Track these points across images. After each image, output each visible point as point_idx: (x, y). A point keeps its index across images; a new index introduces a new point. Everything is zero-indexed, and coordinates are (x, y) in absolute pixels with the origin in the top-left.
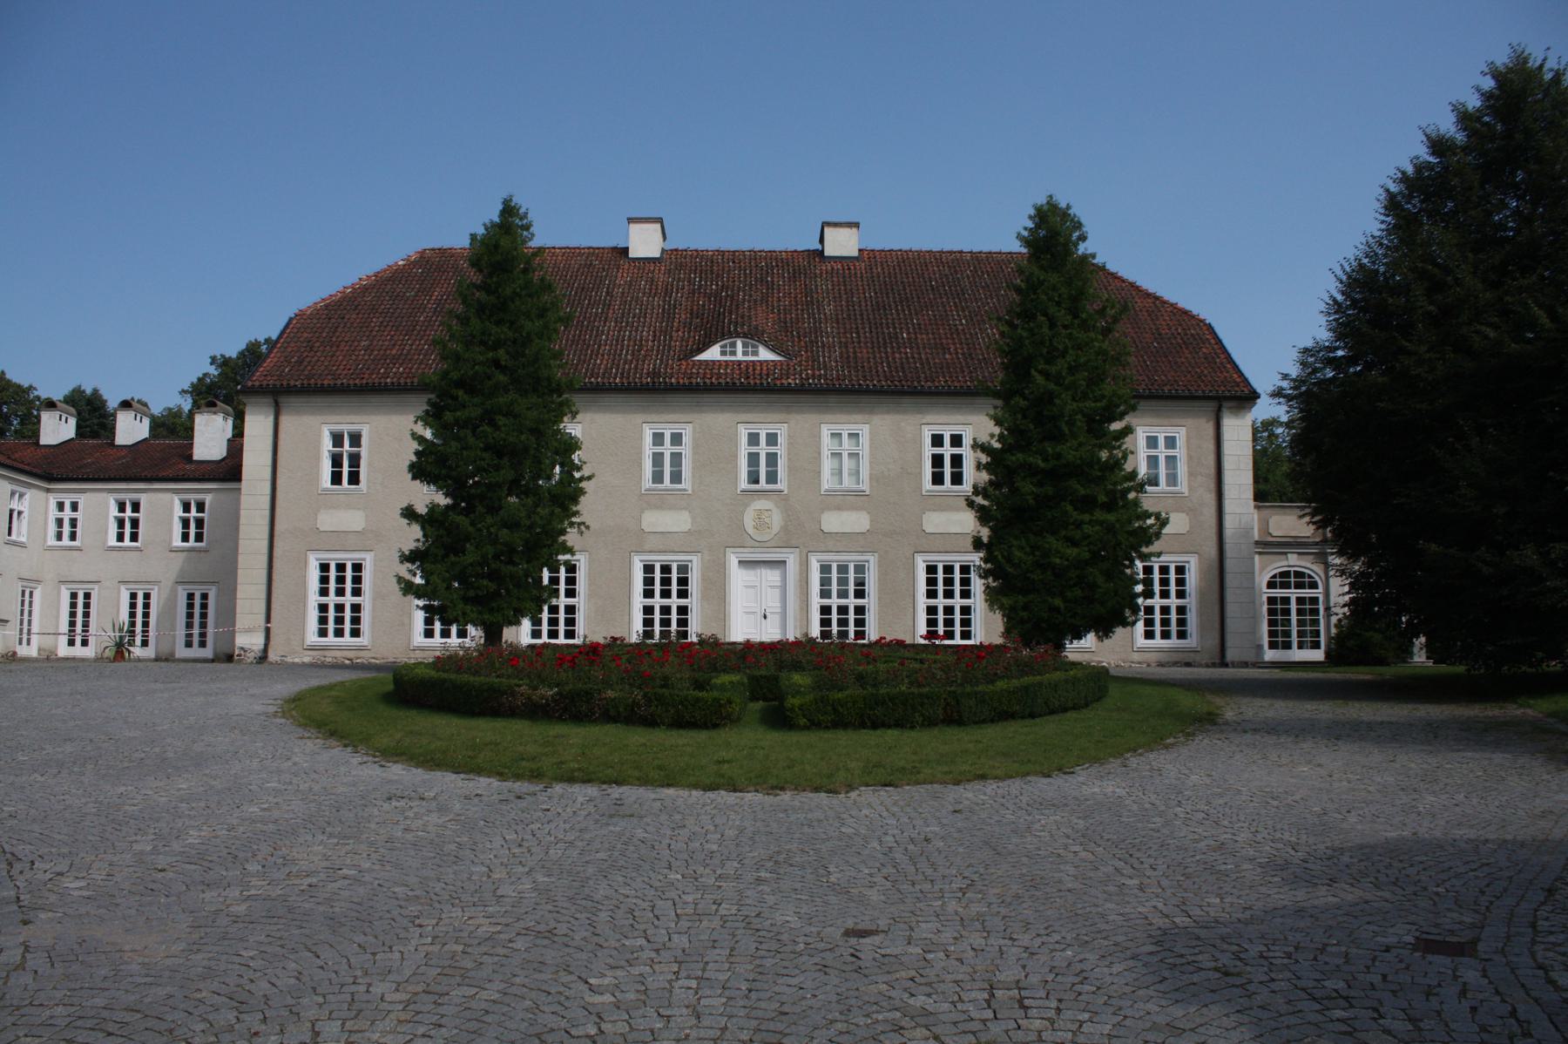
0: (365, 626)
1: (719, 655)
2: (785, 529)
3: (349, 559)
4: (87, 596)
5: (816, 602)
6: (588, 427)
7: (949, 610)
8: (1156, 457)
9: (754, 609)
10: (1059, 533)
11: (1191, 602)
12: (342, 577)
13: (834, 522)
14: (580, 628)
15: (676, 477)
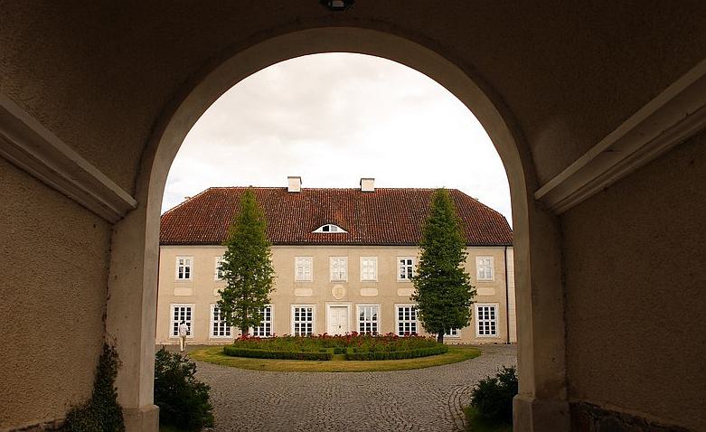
1: (325, 339)
2: (347, 295)
5: (359, 322)
9: (336, 323)
10: (443, 297)
11: (497, 320)
13: (364, 292)
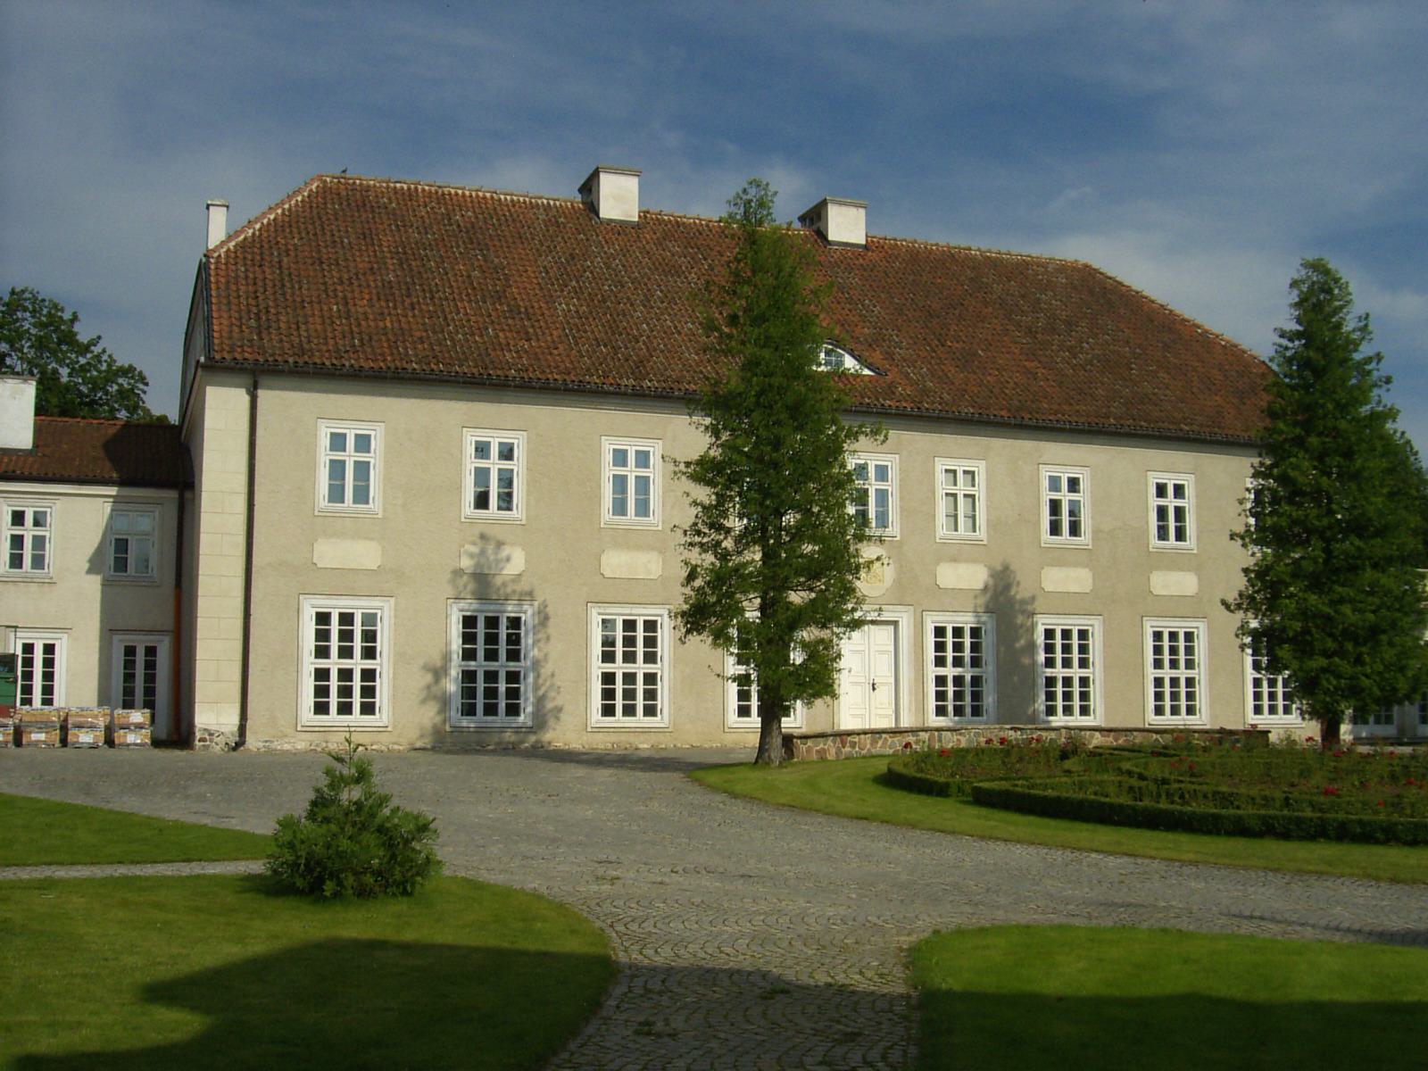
0: (663, 700)
3: (1181, 627)
4: (49, 649)
5: (932, 671)
6: (862, 454)
7: (346, 674)
8: (343, 463)
12: (1174, 648)
14: (60, 698)
15: (362, 495)
